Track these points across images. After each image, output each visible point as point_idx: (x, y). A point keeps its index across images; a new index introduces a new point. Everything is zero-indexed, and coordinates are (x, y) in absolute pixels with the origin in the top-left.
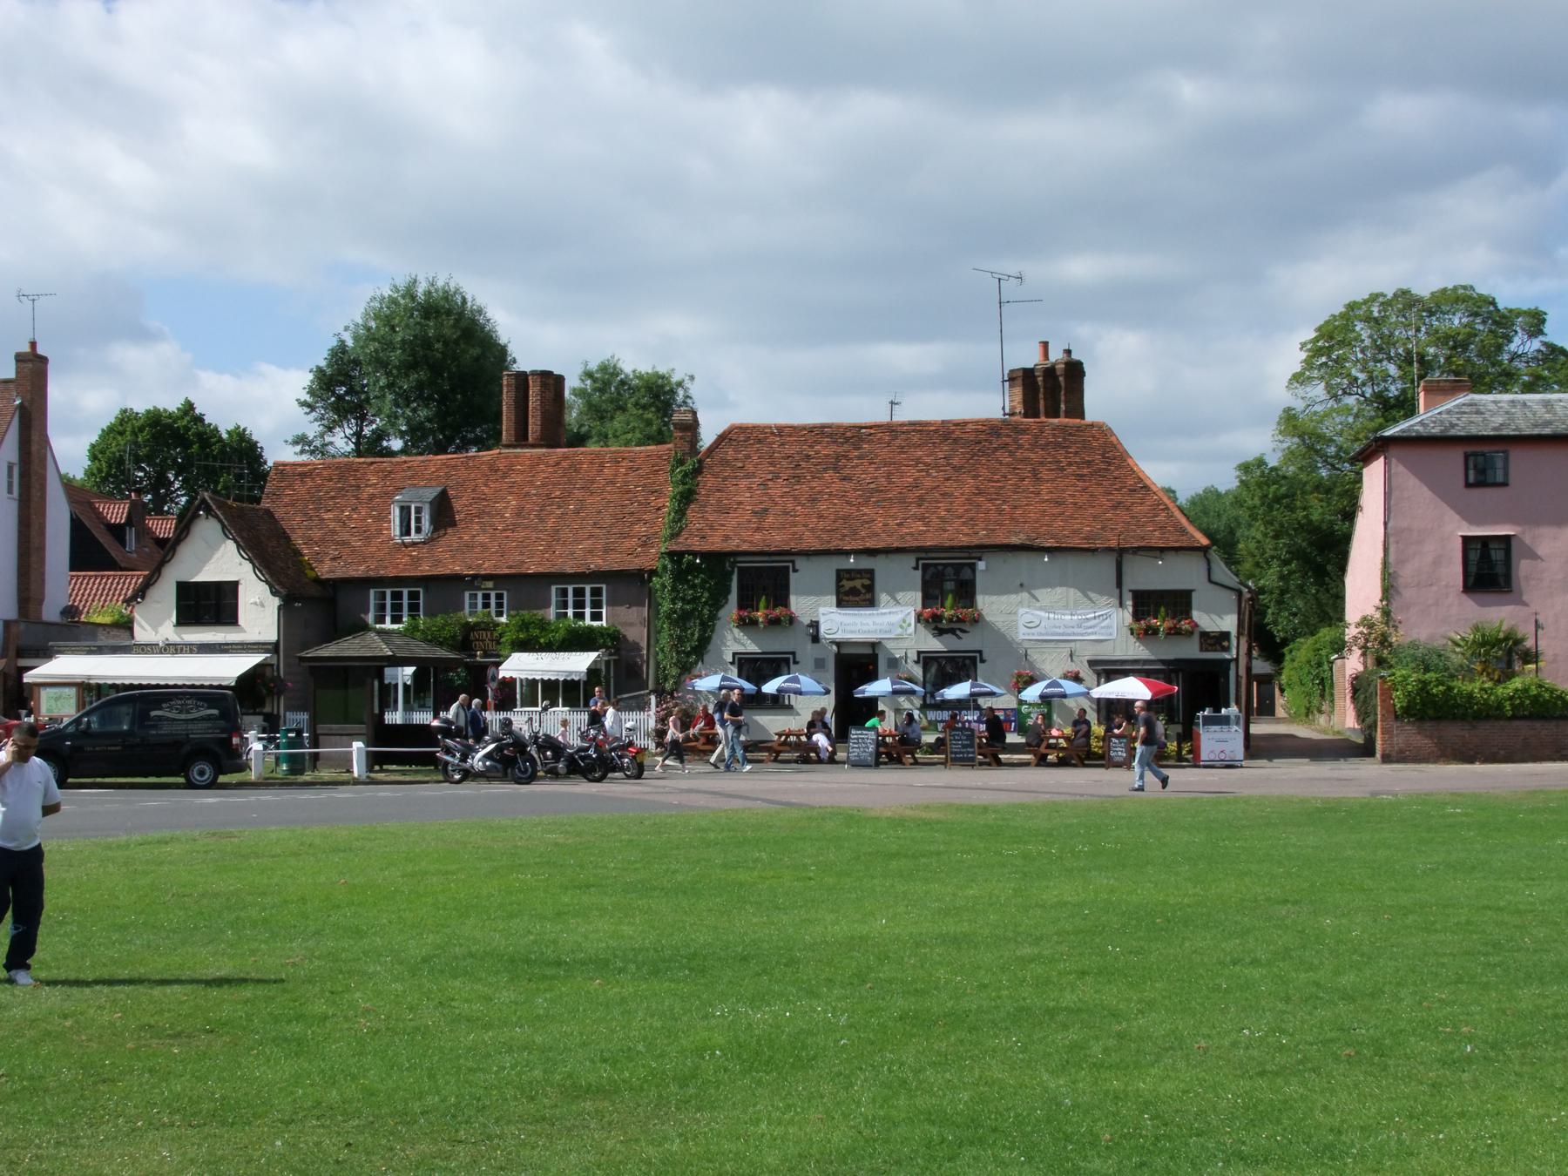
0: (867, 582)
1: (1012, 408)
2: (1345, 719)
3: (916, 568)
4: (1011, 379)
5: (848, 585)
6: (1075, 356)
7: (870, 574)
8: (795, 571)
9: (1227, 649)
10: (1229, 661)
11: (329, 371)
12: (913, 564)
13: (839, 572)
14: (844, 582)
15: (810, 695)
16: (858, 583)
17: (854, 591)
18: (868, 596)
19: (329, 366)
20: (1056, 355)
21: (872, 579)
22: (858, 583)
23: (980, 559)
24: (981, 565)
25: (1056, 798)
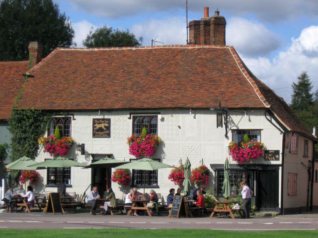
0: (107, 125)
1: (190, 40)
2: (113, 170)
3: (130, 118)
4: (190, 26)
5: (98, 126)
6: (221, 15)
7: (109, 120)
8: (74, 119)
9: (278, 159)
10: (279, 166)
11: (110, 36)
12: (128, 116)
13: (94, 119)
14: (96, 125)
15: (81, 184)
16: (102, 125)
17: (101, 130)
18: (107, 132)
19: (113, 36)
20: (212, 14)
21: (109, 123)
22: (102, 125)
23: (160, 113)
24: (160, 117)
25: (106, 228)
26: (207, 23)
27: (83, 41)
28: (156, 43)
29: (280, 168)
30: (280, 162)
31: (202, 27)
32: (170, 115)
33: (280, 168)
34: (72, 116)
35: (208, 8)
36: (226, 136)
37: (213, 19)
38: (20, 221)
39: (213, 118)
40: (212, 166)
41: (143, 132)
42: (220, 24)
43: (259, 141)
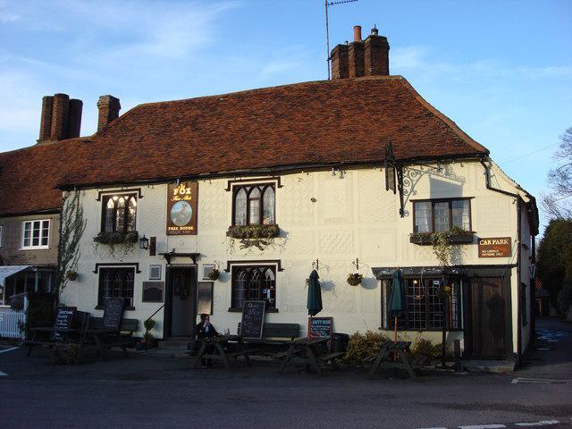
8: (280, 186)
20: (365, 35)
26: (358, 46)
27: (342, 177)
28: (446, 212)
29: (514, 271)
30: (513, 260)
31: (351, 53)
32: (331, 172)
33: (514, 271)
34: (276, 181)
35: (359, 28)
36: (402, 213)
37: (369, 40)
38: (274, 339)
39: (377, 176)
40: (376, 271)
41: (409, 333)
42: (379, 46)
43: (466, 221)
